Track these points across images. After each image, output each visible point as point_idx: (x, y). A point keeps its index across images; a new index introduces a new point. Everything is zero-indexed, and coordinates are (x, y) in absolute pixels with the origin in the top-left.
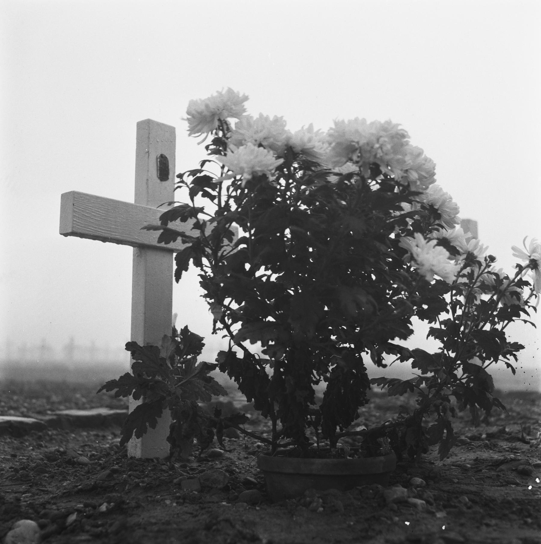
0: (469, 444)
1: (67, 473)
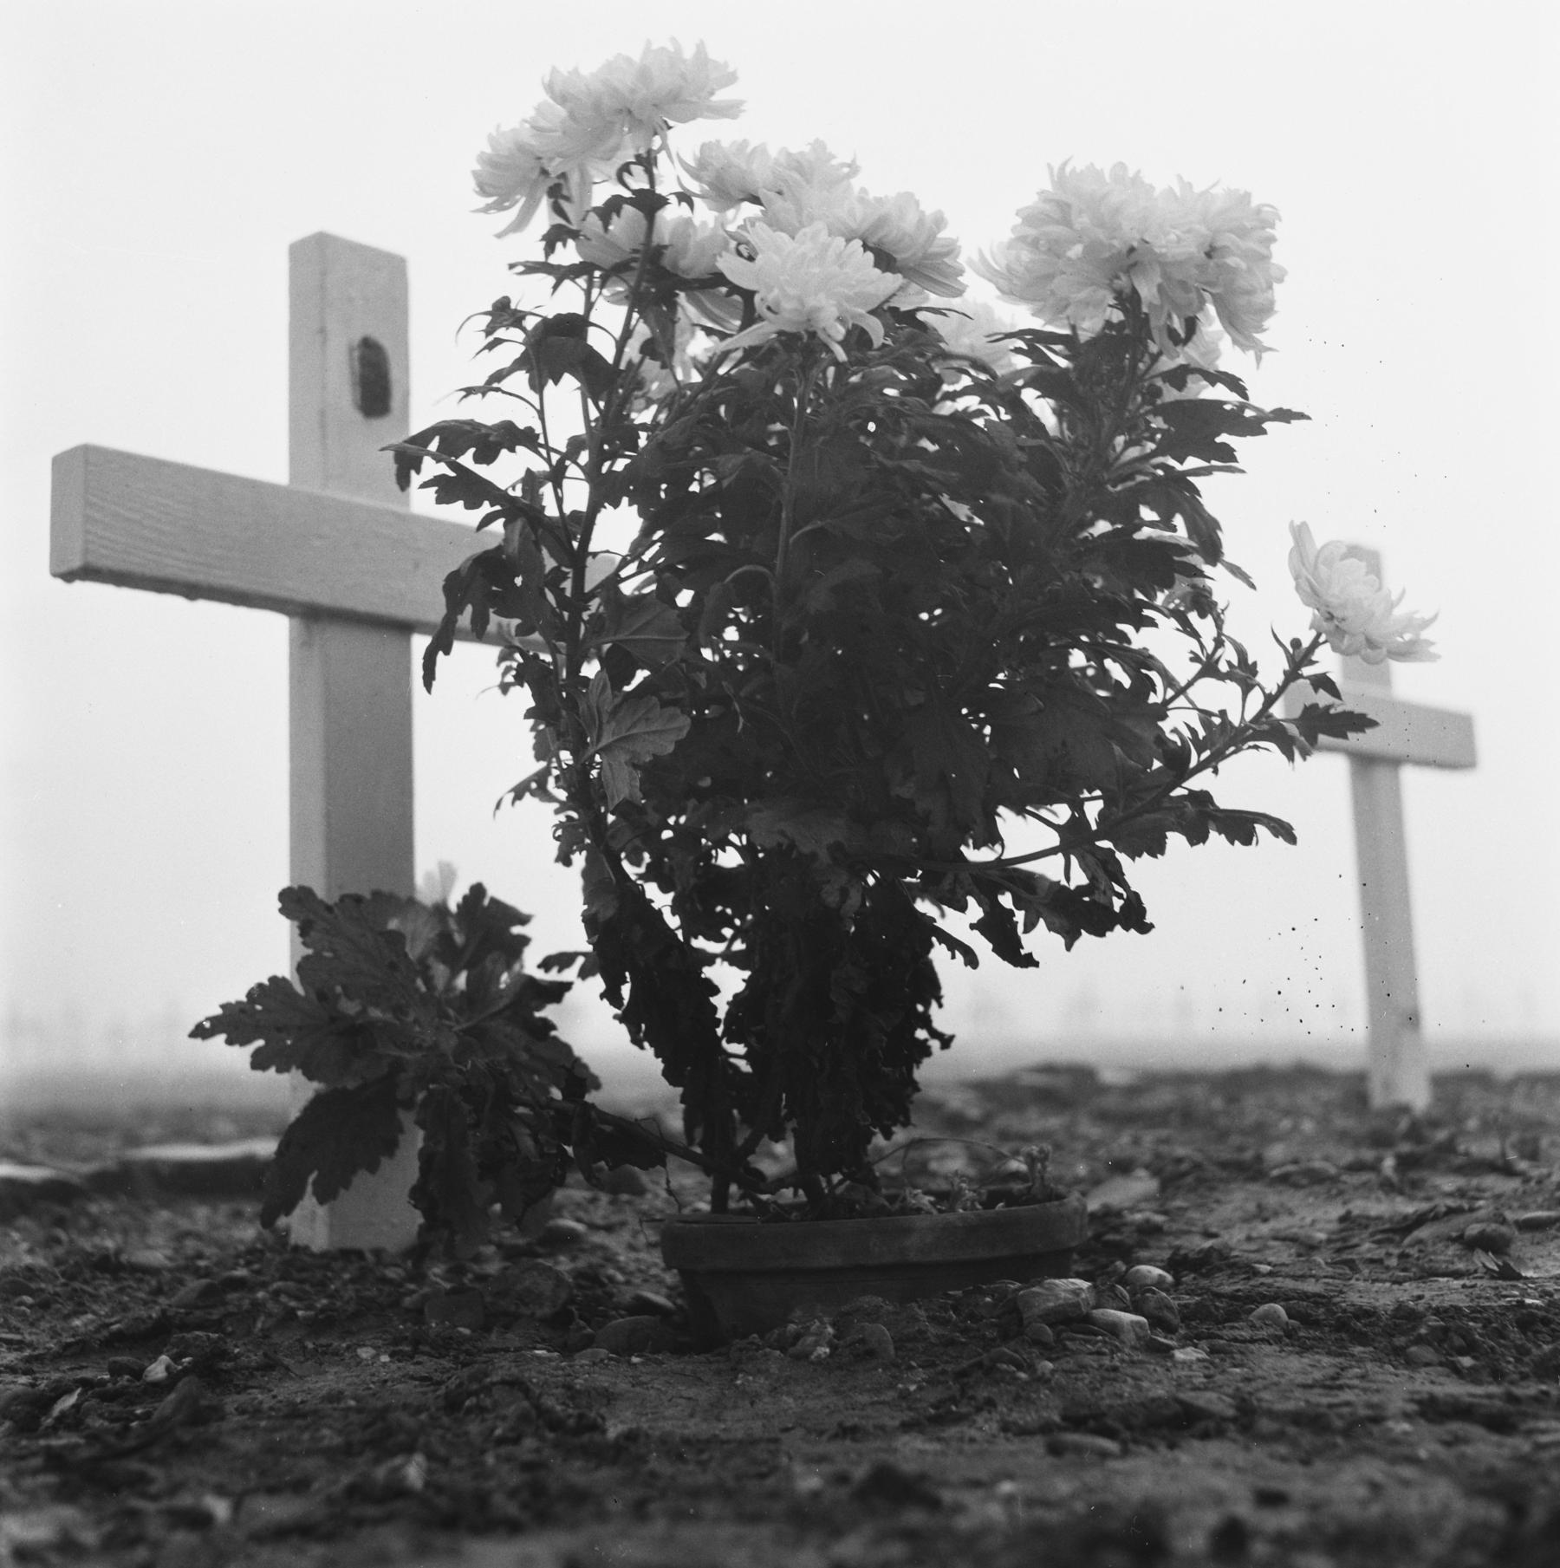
0: (1334, 1180)
1: (91, 1295)
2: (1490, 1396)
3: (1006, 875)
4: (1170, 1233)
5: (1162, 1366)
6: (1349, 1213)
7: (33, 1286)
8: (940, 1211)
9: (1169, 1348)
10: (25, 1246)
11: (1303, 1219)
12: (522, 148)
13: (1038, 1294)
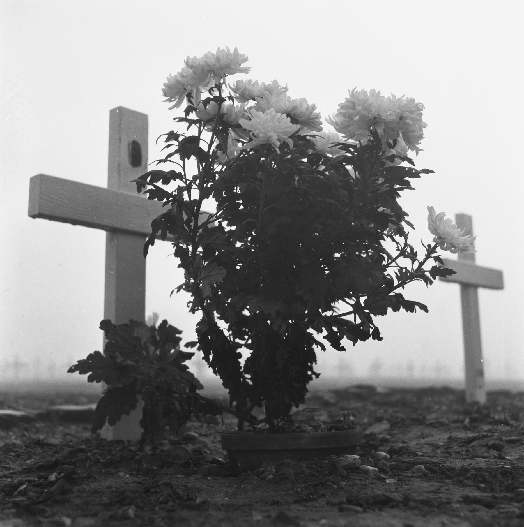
0: (447, 425)
1: (34, 453)
2: (487, 496)
3: (337, 320)
4: (391, 442)
5: (381, 484)
6: (451, 436)
7: (15, 449)
8: (314, 432)
9: (385, 479)
10: (14, 437)
11: (436, 438)
12: (178, 82)
13: (342, 460)
